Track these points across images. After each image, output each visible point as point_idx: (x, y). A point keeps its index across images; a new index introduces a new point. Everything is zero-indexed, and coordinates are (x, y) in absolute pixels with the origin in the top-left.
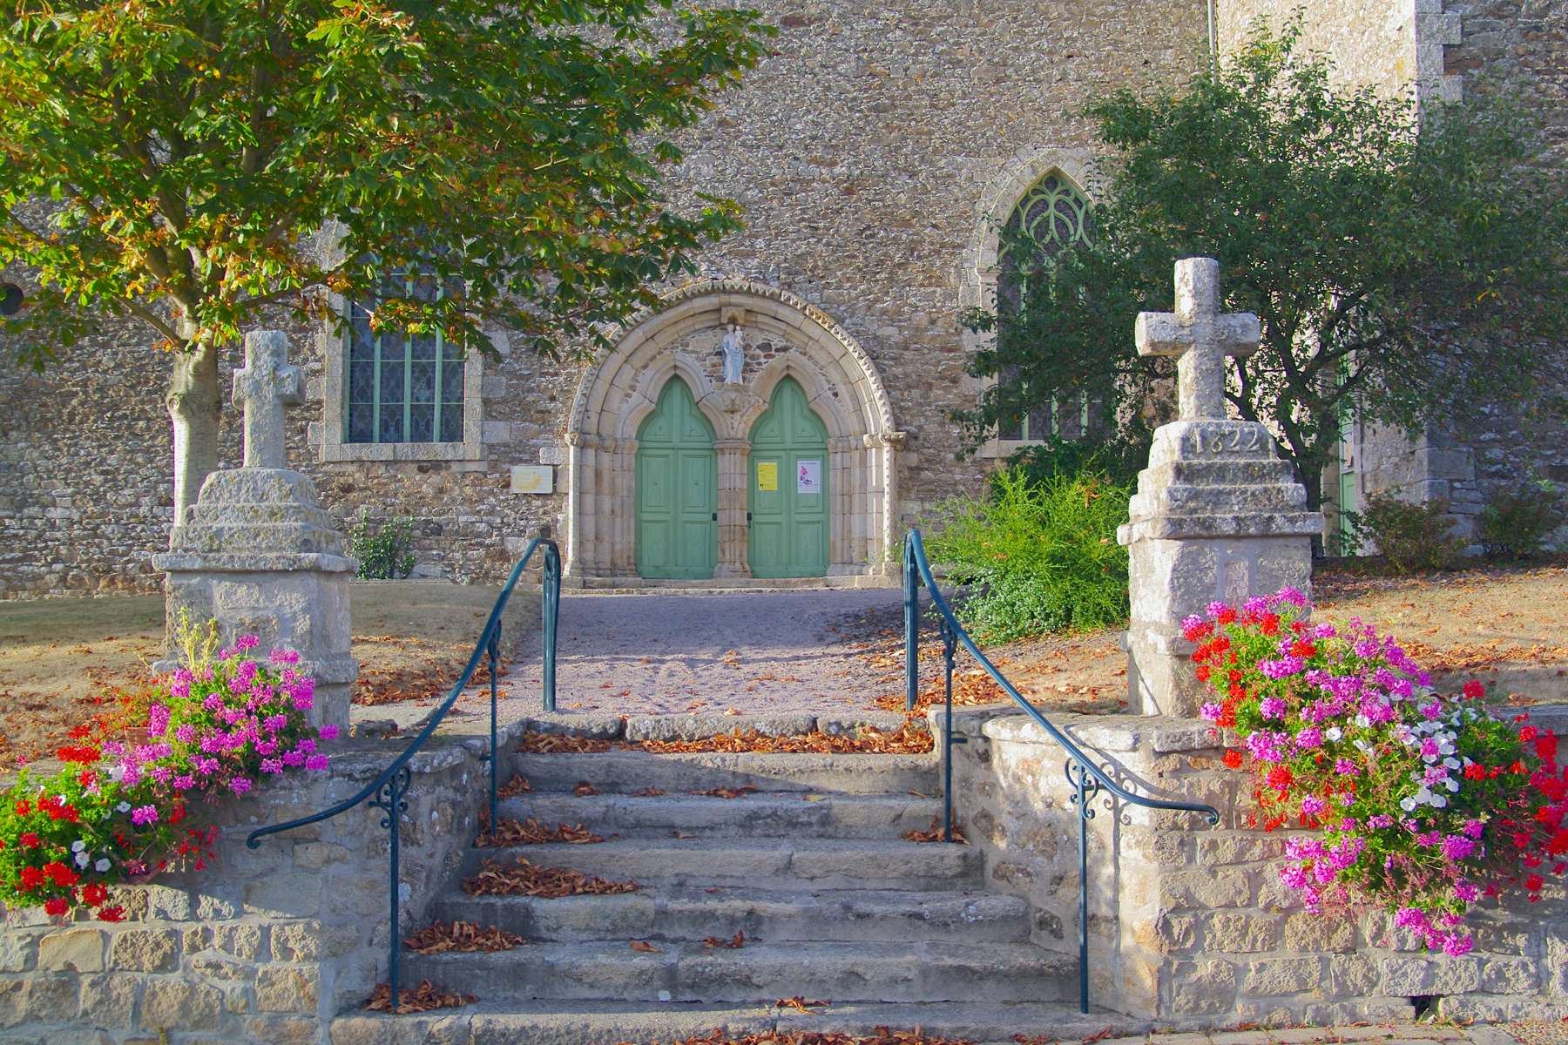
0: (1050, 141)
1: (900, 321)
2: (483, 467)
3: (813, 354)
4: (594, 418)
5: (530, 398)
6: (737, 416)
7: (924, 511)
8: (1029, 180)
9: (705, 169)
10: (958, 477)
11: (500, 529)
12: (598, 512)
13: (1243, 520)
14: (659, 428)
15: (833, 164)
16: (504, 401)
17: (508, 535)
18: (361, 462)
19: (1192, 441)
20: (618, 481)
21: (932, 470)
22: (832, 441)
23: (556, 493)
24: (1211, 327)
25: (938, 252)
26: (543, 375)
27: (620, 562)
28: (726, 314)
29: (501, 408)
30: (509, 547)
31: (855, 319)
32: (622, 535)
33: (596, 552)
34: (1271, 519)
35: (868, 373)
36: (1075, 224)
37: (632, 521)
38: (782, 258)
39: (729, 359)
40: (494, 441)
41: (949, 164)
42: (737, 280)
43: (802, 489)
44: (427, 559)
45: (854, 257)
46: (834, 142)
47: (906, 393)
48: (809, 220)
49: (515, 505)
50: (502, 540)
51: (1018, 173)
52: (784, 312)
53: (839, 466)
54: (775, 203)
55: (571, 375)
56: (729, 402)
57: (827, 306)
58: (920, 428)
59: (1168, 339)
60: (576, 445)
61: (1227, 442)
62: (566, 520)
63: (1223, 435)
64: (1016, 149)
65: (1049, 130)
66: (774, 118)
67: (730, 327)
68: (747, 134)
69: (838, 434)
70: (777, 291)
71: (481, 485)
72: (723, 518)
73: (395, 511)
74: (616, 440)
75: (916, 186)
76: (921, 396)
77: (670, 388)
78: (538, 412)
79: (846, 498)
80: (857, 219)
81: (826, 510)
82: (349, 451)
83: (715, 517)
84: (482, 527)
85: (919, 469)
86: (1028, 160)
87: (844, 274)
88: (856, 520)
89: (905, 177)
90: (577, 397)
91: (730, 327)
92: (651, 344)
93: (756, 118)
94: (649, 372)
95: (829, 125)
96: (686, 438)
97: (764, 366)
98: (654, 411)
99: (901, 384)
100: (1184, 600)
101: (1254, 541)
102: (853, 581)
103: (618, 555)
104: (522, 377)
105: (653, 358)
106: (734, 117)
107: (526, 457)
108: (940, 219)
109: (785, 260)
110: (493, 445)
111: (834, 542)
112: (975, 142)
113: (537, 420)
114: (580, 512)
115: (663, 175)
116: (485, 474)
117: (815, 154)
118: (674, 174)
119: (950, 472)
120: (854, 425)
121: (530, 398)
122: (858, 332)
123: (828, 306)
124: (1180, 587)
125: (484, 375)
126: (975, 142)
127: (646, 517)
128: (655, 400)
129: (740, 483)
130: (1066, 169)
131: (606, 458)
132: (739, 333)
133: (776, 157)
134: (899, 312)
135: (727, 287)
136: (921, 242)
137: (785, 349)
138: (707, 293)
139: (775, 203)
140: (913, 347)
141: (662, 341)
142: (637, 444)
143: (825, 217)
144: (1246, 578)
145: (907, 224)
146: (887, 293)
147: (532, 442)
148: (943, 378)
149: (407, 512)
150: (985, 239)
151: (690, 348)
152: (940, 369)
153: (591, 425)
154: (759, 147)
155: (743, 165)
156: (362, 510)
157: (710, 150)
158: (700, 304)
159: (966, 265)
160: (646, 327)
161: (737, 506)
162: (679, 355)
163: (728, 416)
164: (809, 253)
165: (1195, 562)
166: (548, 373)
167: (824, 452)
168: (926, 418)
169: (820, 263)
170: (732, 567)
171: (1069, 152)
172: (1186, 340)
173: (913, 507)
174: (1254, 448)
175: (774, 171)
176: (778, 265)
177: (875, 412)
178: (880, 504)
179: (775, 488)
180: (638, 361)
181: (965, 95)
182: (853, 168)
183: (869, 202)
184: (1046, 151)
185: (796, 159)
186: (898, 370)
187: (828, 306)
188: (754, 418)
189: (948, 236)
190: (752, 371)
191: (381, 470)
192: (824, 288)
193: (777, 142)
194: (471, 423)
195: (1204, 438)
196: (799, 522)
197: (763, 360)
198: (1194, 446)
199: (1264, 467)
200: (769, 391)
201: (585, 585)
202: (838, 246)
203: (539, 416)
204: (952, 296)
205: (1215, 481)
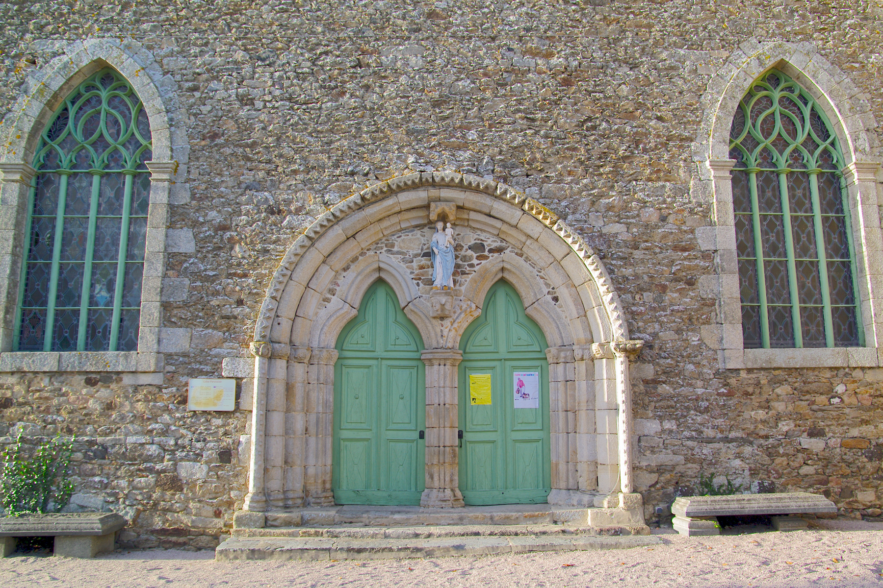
0: (774, 35)
1: (628, 217)
2: (158, 379)
3: (531, 254)
4: (286, 325)
5: (214, 302)
6: (447, 323)
7: (663, 431)
8: (757, 72)
9: (413, 60)
10: (700, 391)
11: (173, 452)
12: (288, 431)
14: (361, 335)
15: (549, 55)
16: (186, 305)
17: (182, 459)
18: (20, 373)
20: (314, 395)
21: (671, 384)
22: (553, 350)
25: (665, 145)
26: (230, 276)
27: (315, 488)
28: (435, 210)
29: (182, 313)
30: (183, 473)
31: (578, 216)
32: (317, 457)
33: (285, 478)
35: (595, 274)
36: (803, 120)
37: (329, 441)
38: (497, 150)
39: (438, 259)
41: (671, 56)
42: (448, 172)
43: (519, 403)
44: (87, 486)
45: (575, 149)
46: (549, 34)
47: (637, 297)
48: (524, 111)
49: (192, 425)
50: (175, 465)
51: (744, 65)
52: (499, 208)
53: (561, 378)
54: (488, 94)
56: (438, 307)
57: (547, 199)
58: (655, 335)
60: (262, 356)
62: (248, 442)
64: (739, 42)
65: (773, 24)
66: (486, 10)
67: (440, 225)
68: (458, 26)
69: (559, 343)
70: (493, 184)
71: (155, 401)
72: (431, 437)
73: (56, 430)
74: (311, 349)
75: (637, 78)
76: (654, 300)
77: (374, 292)
78: (223, 317)
79: (570, 414)
80: (577, 111)
81: (546, 427)
82: (8, 361)
83: (422, 435)
84: (153, 450)
85: (656, 382)
86: (754, 54)
87: (564, 167)
88: (582, 441)
89: (625, 69)
90: (265, 303)
91: (440, 225)
92: (352, 243)
93: (467, 10)
94: (351, 274)
95: (544, 18)
96: (390, 347)
97: (477, 268)
98: (356, 317)
99: (631, 287)
102: (585, 516)
103: (312, 480)
104: (208, 279)
105: (355, 260)
106: (443, 10)
108: (665, 111)
109: (500, 153)
110: (171, 355)
111: (557, 465)
112: (697, 34)
113: (222, 326)
114: (265, 433)
115: (368, 65)
117: (529, 45)
118: (381, 65)
119: (690, 385)
120: (577, 332)
121: (214, 302)
122: (582, 229)
123: (548, 201)
125: (165, 276)
126: (697, 34)
127: (345, 434)
128: (357, 305)
129: (450, 397)
130: (793, 61)
131: (299, 370)
132: (449, 230)
133: (488, 48)
134: (626, 208)
135: (437, 180)
136: (647, 134)
137: (500, 250)
138: (415, 186)
139: (488, 94)
140: (643, 245)
141: (364, 240)
142: (336, 354)
143: (542, 109)
145: (630, 116)
146: (612, 187)
147: (214, 351)
148: (678, 280)
149: (70, 431)
150: (715, 131)
151: (396, 249)
152: (674, 269)
153: (282, 332)
154: (470, 38)
155: (453, 56)
156: (19, 430)
157: (418, 41)
158: (407, 198)
159: (695, 159)
160: (345, 223)
161: (447, 424)
162: (384, 256)
163: (437, 323)
164: (526, 145)
166: (235, 274)
167: (543, 362)
168: (661, 324)
169: (538, 156)
170: (441, 495)
171: (794, 45)
173: (652, 427)
175: (486, 62)
176: (492, 158)
177: (604, 317)
178: (614, 424)
179: (489, 402)
180: (338, 261)
182: (571, 59)
183: (589, 93)
184: (771, 44)
185: (510, 50)
186: (628, 271)
187: (548, 201)
188: (465, 325)
189: (674, 128)
190: (463, 273)
191: (44, 382)
192: (543, 182)
193: (489, 33)
194: (147, 330)
196: (515, 441)
197: (475, 262)
200: (482, 296)
201: (267, 523)
202: (558, 137)
203: (223, 322)
204: (683, 190)
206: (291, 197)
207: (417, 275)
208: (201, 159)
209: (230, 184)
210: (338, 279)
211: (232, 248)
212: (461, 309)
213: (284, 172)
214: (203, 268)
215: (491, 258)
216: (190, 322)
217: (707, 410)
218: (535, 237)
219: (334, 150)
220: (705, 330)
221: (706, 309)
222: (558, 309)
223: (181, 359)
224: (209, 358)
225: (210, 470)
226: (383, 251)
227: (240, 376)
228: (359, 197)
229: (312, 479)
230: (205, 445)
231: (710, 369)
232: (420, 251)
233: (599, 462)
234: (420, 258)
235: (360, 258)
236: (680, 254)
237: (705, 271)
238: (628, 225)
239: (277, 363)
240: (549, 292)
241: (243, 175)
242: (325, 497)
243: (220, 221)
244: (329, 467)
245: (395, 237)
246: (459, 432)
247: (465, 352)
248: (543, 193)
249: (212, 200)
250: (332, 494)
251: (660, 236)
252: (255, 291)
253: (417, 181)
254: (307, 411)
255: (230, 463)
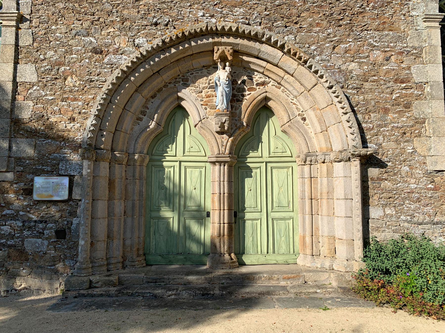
10: (413, 186)
12: (110, 213)
47: (367, 117)
96: (272, 155)
105: (160, 90)
137: (263, 84)
152: (394, 97)
180: (147, 92)
206: (110, 41)
207: (205, 102)
208: (40, 12)
209: (64, 31)
210: (147, 104)
211: (65, 79)
212: (236, 126)
213: (105, 22)
214: (43, 94)
215: (258, 90)
216: (35, 134)
217: (419, 200)
218: (291, 73)
219: (142, 6)
220: (416, 143)
221: (418, 126)
222: (305, 126)
223: (27, 162)
224: (49, 161)
225: (49, 244)
226: (180, 84)
227: (72, 174)
228: (161, 41)
229: (129, 248)
230: (46, 225)
231: (421, 170)
232: (207, 84)
233: (336, 236)
234: (207, 89)
235: (164, 89)
236: (399, 85)
237: (418, 97)
238: (360, 63)
239: (101, 164)
240: (299, 114)
241: (74, 24)
242: (138, 261)
243: (57, 59)
244: (142, 238)
245: (189, 74)
246: (234, 212)
247: (238, 157)
248: (297, 41)
249: (50, 43)
250: (144, 258)
251: (384, 72)
252: (83, 111)
253: (204, 29)
254: (125, 199)
255: (65, 238)
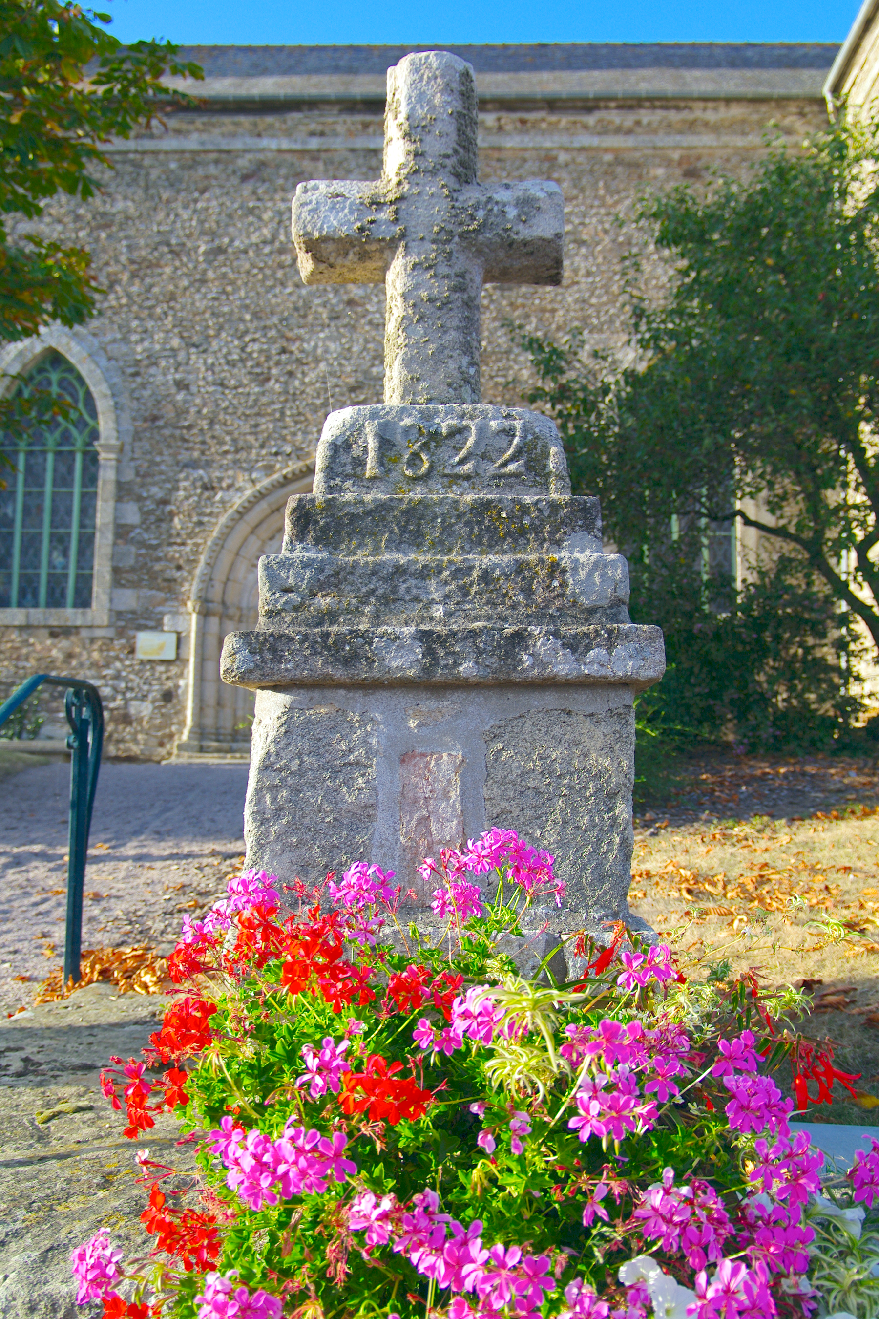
2: (110, 633)
4: (218, 587)
9: (332, 346)
11: (124, 694)
13: (441, 640)
16: (133, 570)
17: (132, 699)
19: (356, 451)
23: (179, 660)
24: (446, 204)
26: (171, 544)
29: (133, 577)
30: (132, 711)
34: (519, 639)
40: (122, 608)
49: (140, 671)
55: (197, 545)
59: (344, 231)
61: (443, 453)
62: (187, 686)
63: (435, 436)
74: (240, 608)
100: (288, 848)
101: (477, 698)
107: (152, 623)
112: (598, 317)
116: (112, 640)
121: (158, 567)
124: (278, 812)
125: (115, 544)
144: (455, 794)
147: (160, 609)
153: (216, 593)
165: (319, 747)
172: (386, 232)
174: (512, 467)
181: (589, 274)
183: (492, 377)
195: (385, 443)
198: (360, 463)
199: (525, 510)
201: (202, 750)
203: (165, 584)
205: (395, 545)
